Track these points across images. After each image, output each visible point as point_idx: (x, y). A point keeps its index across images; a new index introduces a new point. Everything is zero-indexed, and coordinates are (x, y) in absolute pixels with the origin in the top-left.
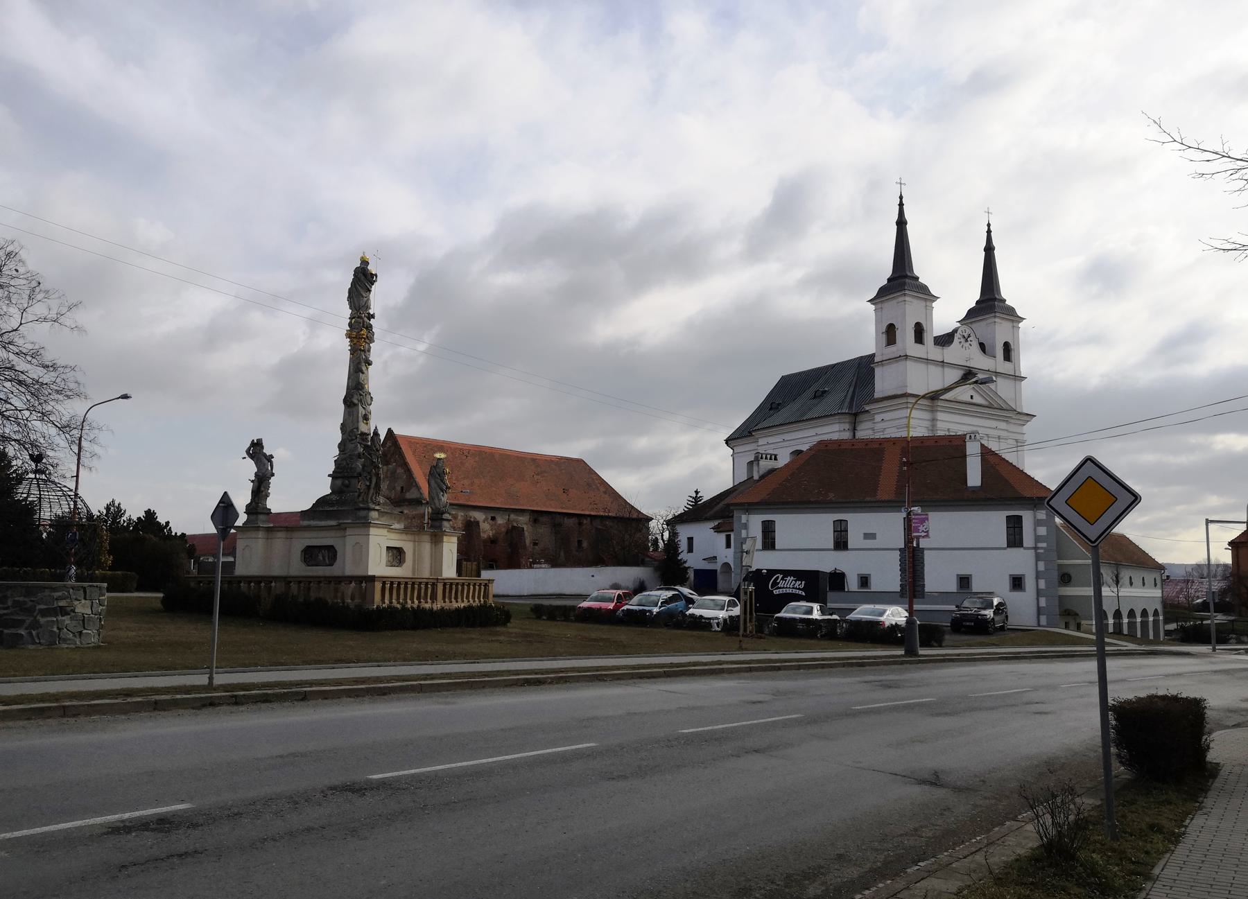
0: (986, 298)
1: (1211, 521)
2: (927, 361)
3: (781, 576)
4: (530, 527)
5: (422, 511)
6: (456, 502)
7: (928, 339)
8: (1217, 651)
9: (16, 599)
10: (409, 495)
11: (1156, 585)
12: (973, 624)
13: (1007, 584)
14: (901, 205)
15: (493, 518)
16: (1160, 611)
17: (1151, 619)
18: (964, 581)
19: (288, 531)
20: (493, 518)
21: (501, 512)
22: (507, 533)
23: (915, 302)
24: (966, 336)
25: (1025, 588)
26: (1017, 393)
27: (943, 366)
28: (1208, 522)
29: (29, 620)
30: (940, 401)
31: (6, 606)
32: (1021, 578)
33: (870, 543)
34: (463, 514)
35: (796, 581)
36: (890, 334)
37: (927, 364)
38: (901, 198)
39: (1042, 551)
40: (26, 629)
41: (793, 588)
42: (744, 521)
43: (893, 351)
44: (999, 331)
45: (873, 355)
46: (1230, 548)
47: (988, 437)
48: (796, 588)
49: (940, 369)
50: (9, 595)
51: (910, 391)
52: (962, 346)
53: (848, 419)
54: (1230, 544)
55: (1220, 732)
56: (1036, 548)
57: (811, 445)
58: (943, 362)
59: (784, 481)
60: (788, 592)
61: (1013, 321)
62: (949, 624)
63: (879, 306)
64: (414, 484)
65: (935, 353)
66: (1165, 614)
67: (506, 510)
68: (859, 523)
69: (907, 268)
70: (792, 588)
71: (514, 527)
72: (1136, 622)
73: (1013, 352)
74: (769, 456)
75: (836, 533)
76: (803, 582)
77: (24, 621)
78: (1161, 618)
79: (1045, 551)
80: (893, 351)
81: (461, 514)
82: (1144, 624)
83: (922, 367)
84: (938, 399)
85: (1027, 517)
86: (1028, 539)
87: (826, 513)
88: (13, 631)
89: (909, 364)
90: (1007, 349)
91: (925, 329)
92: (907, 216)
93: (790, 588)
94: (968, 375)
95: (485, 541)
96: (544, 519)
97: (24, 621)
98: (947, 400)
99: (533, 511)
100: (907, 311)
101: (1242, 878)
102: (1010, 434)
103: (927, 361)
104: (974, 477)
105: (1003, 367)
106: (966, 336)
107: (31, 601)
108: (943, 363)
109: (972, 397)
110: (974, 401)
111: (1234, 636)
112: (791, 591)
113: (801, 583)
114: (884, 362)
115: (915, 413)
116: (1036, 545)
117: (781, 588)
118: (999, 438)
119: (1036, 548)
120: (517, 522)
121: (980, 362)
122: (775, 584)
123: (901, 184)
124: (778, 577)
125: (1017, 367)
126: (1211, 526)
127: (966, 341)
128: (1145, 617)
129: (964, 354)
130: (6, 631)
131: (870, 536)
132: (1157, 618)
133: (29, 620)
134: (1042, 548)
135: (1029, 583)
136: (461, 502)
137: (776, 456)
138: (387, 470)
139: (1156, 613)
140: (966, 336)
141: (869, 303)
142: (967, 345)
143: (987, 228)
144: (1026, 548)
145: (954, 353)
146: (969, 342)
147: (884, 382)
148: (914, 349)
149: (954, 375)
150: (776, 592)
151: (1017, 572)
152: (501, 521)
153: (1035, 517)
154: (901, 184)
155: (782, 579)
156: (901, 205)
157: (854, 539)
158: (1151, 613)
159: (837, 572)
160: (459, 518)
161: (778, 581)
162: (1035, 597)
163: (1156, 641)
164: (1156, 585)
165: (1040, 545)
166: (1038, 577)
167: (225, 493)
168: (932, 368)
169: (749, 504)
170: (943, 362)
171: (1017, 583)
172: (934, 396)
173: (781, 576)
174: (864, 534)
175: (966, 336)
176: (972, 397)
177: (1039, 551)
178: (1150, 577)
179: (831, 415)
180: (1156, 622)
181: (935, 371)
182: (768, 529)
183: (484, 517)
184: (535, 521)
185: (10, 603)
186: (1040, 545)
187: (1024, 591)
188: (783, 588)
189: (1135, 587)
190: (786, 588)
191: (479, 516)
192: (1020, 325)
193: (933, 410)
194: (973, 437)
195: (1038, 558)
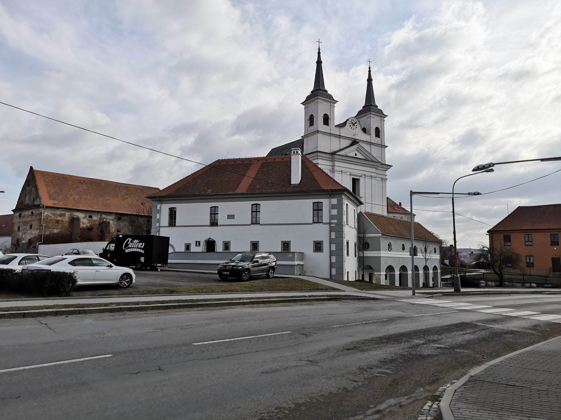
1: (414, 192)
2: (330, 134)
3: (130, 240)
4: (115, 222)
5: (41, 212)
6: (65, 207)
8: (416, 294)
10: (36, 203)
12: (229, 273)
13: (311, 247)
15: (90, 217)
16: (438, 266)
18: (286, 245)
20: (90, 217)
21: (96, 213)
22: (99, 225)
23: (324, 103)
24: (354, 122)
26: (383, 155)
27: (340, 138)
28: (412, 193)
30: (336, 155)
33: (231, 221)
34: (69, 214)
35: (139, 243)
36: (311, 120)
37: (331, 136)
38: (319, 49)
39: (334, 225)
41: (137, 248)
42: (158, 208)
43: (312, 129)
44: (374, 122)
46: (488, 234)
47: (365, 176)
48: (139, 248)
49: (330, 137)
52: (351, 128)
54: (488, 232)
56: (330, 223)
58: (340, 135)
59: (186, 183)
60: (134, 251)
61: (381, 117)
62: (216, 272)
64: (38, 196)
66: (441, 268)
67: (99, 212)
69: (321, 85)
70: (137, 248)
71: (104, 222)
76: (144, 244)
78: (439, 271)
79: (532, 263)
81: (68, 214)
83: (327, 137)
85: (326, 202)
86: (326, 219)
89: (320, 135)
90: (378, 133)
91: (330, 117)
92: (322, 59)
93: (135, 248)
94: (354, 142)
95: (83, 229)
96: (125, 218)
98: (340, 155)
99: (116, 213)
100: (322, 108)
101: (518, 397)
102: (377, 175)
103: (330, 134)
104: (296, 178)
105: (374, 140)
106: (354, 122)
108: (340, 136)
109: (356, 155)
110: (357, 157)
111: (483, 282)
112: (136, 251)
113: (142, 245)
114: (308, 135)
116: (330, 221)
117: (130, 248)
119: (330, 223)
120: (106, 219)
121: (361, 136)
122: (127, 245)
123: (319, 42)
124: (129, 240)
125: (383, 140)
126: (414, 196)
127: (354, 125)
131: (231, 217)
135: (326, 246)
136: (69, 207)
138: (29, 189)
139: (435, 268)
140: (354, 123)
141: (302, 105)
142: (354, 127)
143: (369, 69)
146: (356, 126)
149: (347, 143)
150: (127, 251)
151: (318, 239)
152: (95, 218)
154: (319, 42)
155: (131, 242)
156: (319, 53)
157: (222, 218)
159: (210, 240)
160: (67, 215)
161: (129, 243)
162: (329, 256)
163: (435, 286)
165: (333, 221)
166: (331, 243)
167: (12, 210)
168: (333, 138)
170: (340, 135)
171: (318, 247)
172: (333, 154)
173: (130, 240)
174: (228, 215)
175: (354, 123)
176: (356, 155)
177: (332, 225)
180: (435, 274)
181: (335, 140)
182: (173, 213)
183: (84, 216)
184: (119, 219)
186: (333, 221)
188: (132, 248)
189: (394, 251)
190: (133, 248)
191: (80, 215)
193: (333, 161)
194: (295, 152)
195: (331, 230)
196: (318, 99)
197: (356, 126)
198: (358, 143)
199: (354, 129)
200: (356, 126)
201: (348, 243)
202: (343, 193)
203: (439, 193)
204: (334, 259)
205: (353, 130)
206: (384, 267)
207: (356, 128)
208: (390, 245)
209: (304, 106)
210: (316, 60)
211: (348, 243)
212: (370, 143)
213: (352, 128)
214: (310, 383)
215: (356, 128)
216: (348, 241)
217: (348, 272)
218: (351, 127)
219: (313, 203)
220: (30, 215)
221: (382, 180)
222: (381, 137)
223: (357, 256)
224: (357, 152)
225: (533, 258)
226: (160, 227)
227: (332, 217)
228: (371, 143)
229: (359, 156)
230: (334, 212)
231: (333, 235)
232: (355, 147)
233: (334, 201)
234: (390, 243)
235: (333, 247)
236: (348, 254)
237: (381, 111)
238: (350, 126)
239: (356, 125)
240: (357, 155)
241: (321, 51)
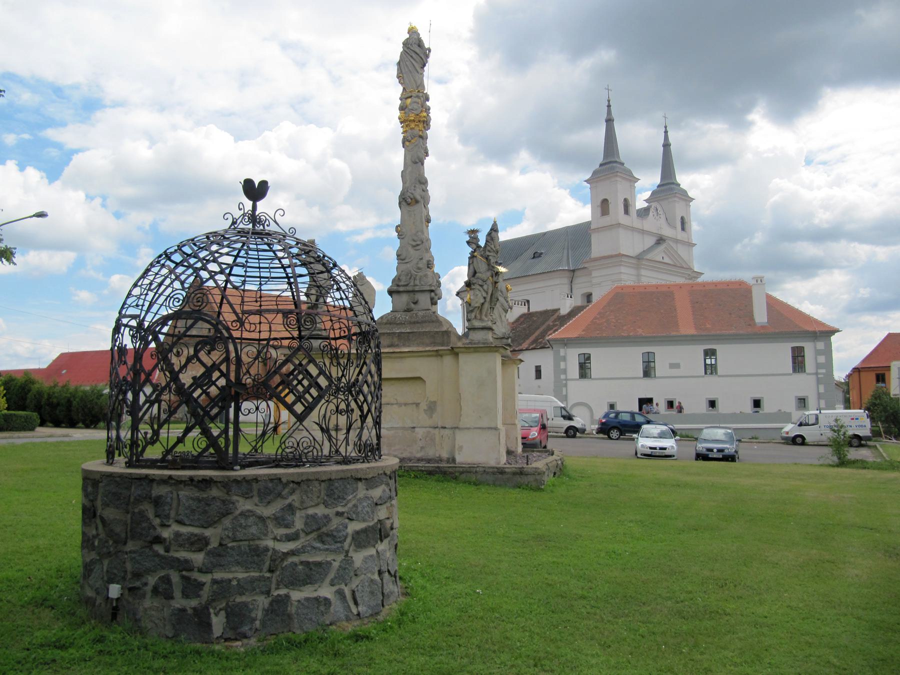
7: (633, 213)
9: (311, 511)
14: (609, 106)
19: (441, 356)
25: (752, 402)
29: (337, 561)
31: (293, 530)
36: (604, 207)
38: (609, 101)
39: (822, 376)
40: (332, 584)
43: (607, 220)
45: (589, 223)
50: (297, 504)
51: (622, 252)
53: (568, 274)
55: (90, 462)
56: (817, 374)
57: (660, 282)
65: (637, 223)
68: (664, 355)
74: (520, 303)
75: (802, 355)
77: (329, 564)
80: (607, 220)
84: (643, 259)
87: (605, 347)
88: (307, 592)
94: (660, 240)
97: (329, 564)
100: (617, 192)
104: (761, 316)
105: (680, 235)
107: (339, 514)
115: (623, 269)
119: (817, 374)
123: (608, 90)
129: (655, 224)
130: (296, 595)
133: (337, 561)
134: (821, 374)
137: (528, 301)
145: (651, 224)
147: (599, 246)
148: (623, 219)
149: (650, 241)
153: (815, 348)
154: (608, 90)
157: (661, 367)
165: (820, 371)
169: (569, 339)
172: (639, 258)
177: (819, 376)
179: (554, 271)
185: (299, 524)
195: (819, 382)
198: (664, 240)
209: (589, 185)
214: (165, 625)
224: (664, 256)
225: (818, 390)
226: (566, 380)
227: (818, 366)
229: (667, 260)
230: (822, 359)
232: (662, 247)
233: (821, 345)
237: (686, 192)
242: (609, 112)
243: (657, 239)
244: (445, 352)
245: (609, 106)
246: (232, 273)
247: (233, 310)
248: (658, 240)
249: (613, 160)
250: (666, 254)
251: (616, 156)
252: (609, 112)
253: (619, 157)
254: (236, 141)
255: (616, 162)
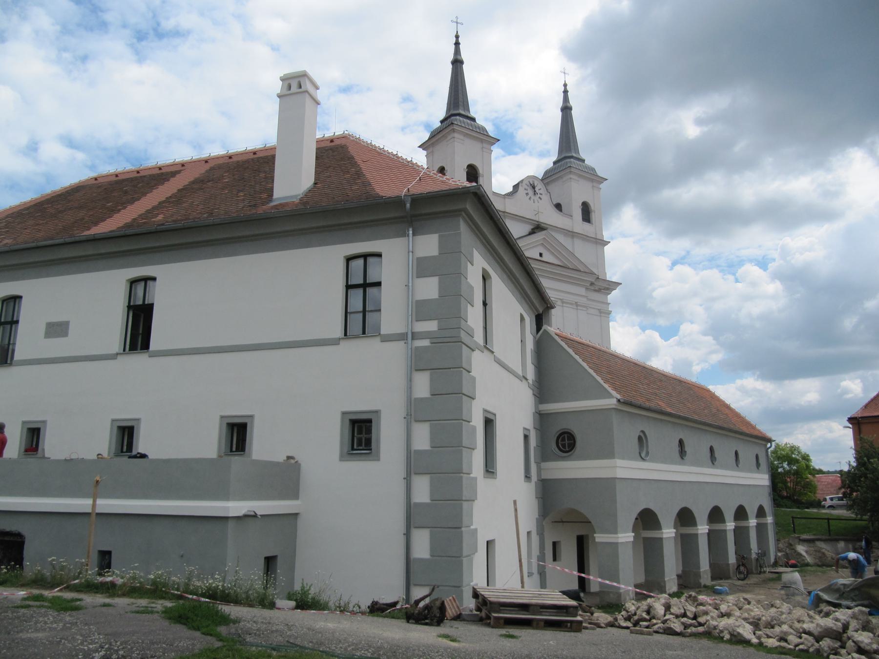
0: (563, 156)
11: (758, 465)
14: (457, 44)
17: (730, 525)
32: (369, 421)
38: (457, 37)
39: (426, 343)
46: (851, 426)
47: (563, 302)
63: (431, 149)
72: (696, 535)
73: (593, 213)
82: (741, 534)
90: (586, 213)
92: (464, 56)
109: (541, 255)
110: (543, 259)
118: (577, 304)
121: (550, 217)
128: (646, 540)
131: (57, 329)
132: (762, 521)
139: (761, 512)
144: (388, 339)
146: (539, 195)
151: (360, 405)
158: (729, 514)
162: (402, 474)
164: (758, 465)
176: (541, 255)
178: (747, 452)
187: (342, 458)
189: (722, 467)
192: (601, 186)
196: (454, 132)
197: (541, 196)
199: (536, 201)
200: (541, 196)
201: (489, 423)
202: (460, 210)
203: (520, 561)
204: (422, 491)
205: (534, 202)
206: (627, 516)
207: (541, 199)
208: (642, 440)
209: (425, 153)
210: (451, 57)
211: (489, 423)
212: (571, 234)
213: (532, 200)
215: (541, 199)
216: (490, 417)
217: (489, 544)
218: (529, 197)
219: (349, 259)
220: (287, 460)
221: (601, 312)
222: (593, 223)
223: (534, 477)
227: (421, 310)
228: (572, 234)
231: (422, 386)
232: (539, 236)
234: (643, 432)
235: (422, 438)
236: (490, 468)
238: (527, 194)
239: (540, 194)
240: (544, 255)
241: (460, 40)
242: (457, 51)
243: (532, 227)
244: (11, 314)
245: (457, 44)
246: (830, 521)
247: (541, 471)
248: (532, 229)
249: (570, 155)
250: (546, 248)
251: (573, 151)
252: (457, 51)
253: (577, 151)
254: (552, 307)
255: (572, 157)
